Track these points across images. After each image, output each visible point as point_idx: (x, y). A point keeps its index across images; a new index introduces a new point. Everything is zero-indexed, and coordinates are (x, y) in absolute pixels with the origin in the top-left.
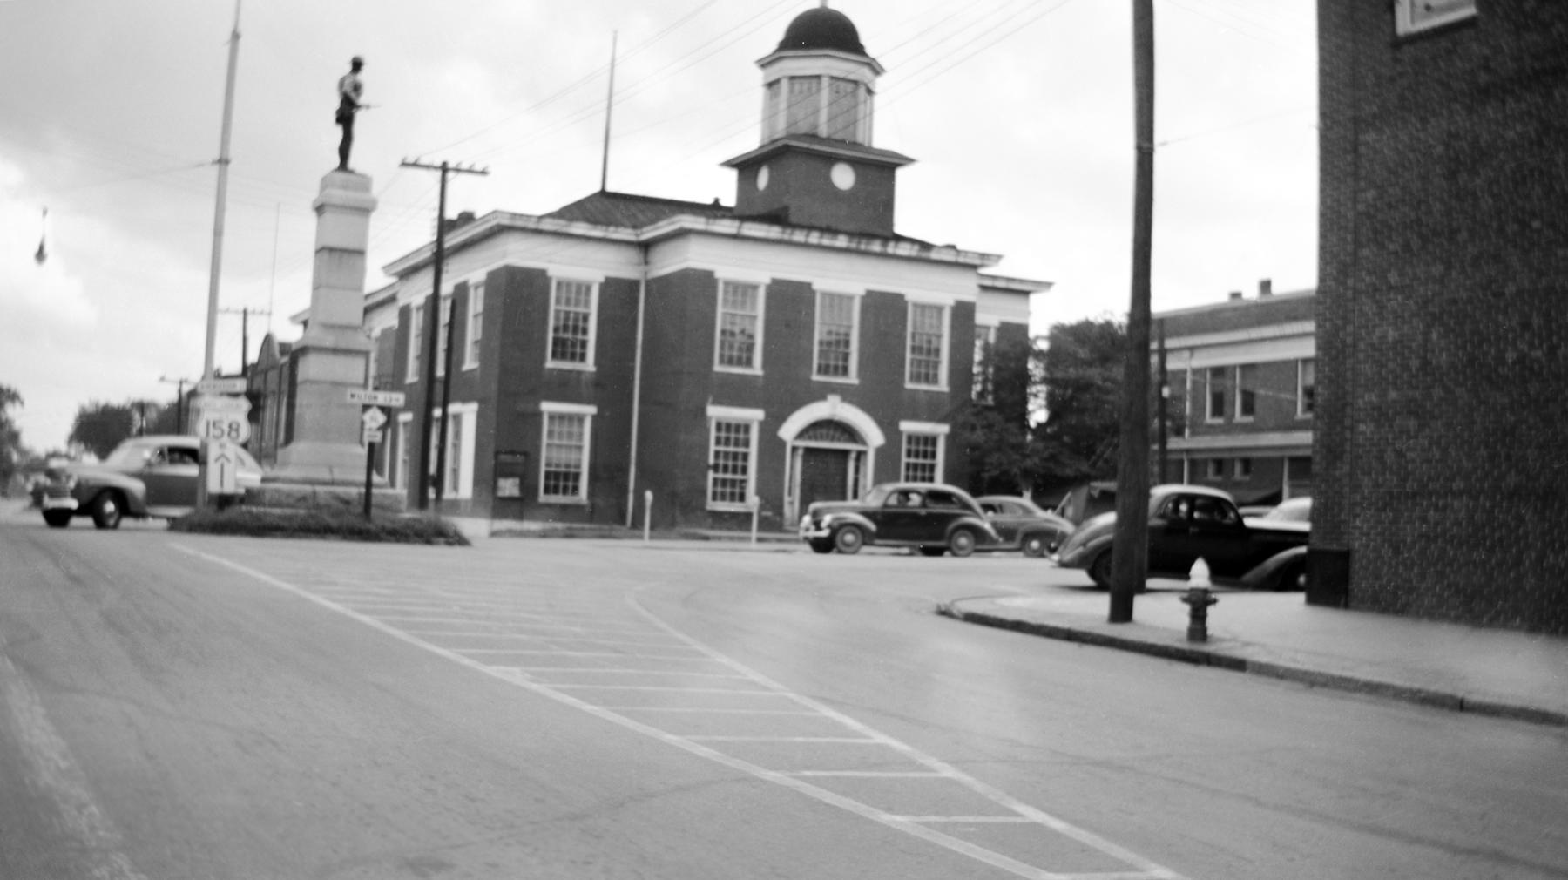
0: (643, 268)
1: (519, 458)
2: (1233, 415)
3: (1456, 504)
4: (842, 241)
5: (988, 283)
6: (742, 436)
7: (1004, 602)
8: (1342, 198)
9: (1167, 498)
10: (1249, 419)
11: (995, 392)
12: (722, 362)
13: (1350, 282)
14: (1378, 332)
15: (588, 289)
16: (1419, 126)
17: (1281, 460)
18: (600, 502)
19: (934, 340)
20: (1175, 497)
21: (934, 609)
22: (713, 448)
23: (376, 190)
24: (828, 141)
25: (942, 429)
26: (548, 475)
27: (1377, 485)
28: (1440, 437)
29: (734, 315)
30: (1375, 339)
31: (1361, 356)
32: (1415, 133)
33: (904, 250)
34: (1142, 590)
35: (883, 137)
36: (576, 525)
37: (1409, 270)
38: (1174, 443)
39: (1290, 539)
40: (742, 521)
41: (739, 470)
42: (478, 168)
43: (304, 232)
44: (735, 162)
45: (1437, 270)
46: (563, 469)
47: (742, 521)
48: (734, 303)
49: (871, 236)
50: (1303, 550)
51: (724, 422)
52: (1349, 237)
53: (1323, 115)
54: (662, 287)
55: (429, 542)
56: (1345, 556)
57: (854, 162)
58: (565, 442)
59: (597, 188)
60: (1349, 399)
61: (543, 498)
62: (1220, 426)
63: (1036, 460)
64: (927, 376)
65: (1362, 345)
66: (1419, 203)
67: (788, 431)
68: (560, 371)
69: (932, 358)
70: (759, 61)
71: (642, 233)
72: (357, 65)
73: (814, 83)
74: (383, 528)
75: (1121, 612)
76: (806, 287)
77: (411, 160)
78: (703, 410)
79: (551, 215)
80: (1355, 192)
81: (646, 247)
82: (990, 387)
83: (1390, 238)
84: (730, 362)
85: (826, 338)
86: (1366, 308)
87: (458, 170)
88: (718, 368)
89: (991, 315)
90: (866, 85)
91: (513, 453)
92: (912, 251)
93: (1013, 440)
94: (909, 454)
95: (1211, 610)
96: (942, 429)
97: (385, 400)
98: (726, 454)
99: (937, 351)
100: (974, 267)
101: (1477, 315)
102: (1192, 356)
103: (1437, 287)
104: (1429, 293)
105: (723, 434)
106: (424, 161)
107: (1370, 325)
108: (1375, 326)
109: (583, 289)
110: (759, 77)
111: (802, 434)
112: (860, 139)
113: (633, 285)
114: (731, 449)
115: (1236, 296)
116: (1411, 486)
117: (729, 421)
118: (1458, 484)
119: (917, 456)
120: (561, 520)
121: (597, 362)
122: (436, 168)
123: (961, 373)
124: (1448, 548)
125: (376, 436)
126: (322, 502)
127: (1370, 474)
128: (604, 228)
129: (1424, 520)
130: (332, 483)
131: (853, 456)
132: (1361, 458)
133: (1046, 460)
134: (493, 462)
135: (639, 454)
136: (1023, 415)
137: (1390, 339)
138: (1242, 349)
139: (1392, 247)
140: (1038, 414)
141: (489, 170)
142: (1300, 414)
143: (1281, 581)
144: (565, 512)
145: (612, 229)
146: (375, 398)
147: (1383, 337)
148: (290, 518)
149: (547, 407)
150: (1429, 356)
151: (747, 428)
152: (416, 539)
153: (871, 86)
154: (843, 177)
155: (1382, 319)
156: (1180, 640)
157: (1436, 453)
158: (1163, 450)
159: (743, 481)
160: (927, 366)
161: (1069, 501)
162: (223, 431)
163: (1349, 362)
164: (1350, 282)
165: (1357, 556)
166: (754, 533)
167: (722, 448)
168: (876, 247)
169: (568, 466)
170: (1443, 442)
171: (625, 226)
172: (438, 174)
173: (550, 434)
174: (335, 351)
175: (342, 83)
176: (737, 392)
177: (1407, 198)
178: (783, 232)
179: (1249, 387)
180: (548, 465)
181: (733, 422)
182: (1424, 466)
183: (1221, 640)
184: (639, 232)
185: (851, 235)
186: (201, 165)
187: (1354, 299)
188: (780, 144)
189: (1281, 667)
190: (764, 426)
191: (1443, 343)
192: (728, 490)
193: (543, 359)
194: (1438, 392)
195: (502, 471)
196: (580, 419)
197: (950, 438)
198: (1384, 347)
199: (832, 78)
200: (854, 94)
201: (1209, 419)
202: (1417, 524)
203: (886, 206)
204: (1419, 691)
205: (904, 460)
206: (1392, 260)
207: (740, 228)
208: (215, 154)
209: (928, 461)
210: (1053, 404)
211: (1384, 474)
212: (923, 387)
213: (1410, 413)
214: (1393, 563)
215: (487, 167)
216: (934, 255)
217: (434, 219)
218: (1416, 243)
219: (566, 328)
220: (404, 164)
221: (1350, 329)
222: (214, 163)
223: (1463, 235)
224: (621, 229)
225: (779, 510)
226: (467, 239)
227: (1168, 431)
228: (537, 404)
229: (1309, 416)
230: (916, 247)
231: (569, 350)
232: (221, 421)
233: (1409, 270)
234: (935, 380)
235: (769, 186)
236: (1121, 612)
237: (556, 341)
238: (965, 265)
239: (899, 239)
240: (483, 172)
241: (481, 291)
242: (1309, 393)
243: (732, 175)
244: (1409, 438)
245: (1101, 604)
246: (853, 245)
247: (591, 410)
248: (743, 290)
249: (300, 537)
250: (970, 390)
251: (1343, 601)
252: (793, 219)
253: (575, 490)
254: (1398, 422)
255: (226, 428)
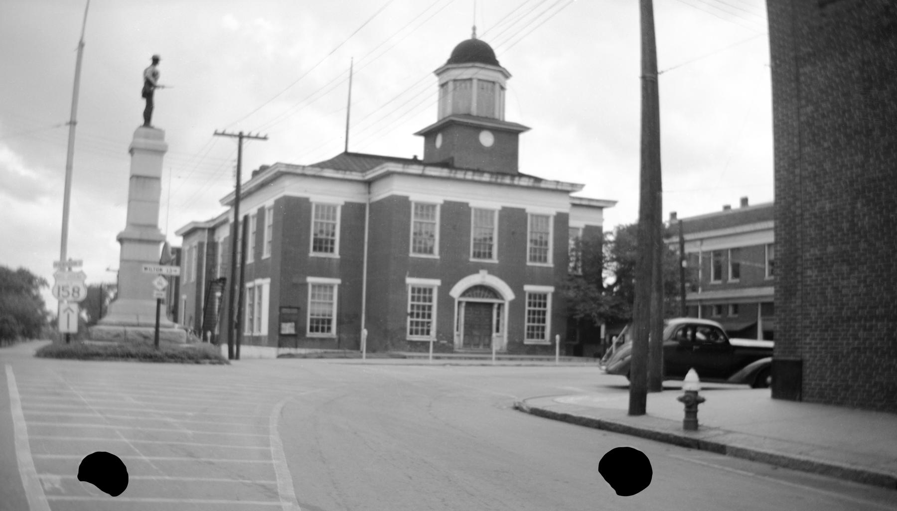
0: (367, 196)
1: (295, 311)
2: (727, 279)
3: (879, 324)
4: (486, 177)
5: (577, 202)
6: (427, 295)
7: (561, 400)
8: (789, 113)
9: (678, 327)
10: (737, 281)
11: (583, 266)
12: (414, 251)
13: (797, 171)
14: (818, 205)
15: (335, 211)
16: (841, 58)
17: (757, 304)
18: (344, 336)
19: (544, 236)
20: (684, 326)
21: (512, 405)
22: (410, 303)
23: (167, 139)
24: (477, 118)
25: (549, 290)
26: (312, 320)
27: (821, 313)
28: (866, 277)
29: (421, 223)
30: (816, 210)
31: (807, 222)
32: (838, 62)
33: (524, 182)
34: (658, 388)
35: (511, 115)
36: (329, 350)
37: (838, 160)
38: (690, 296)
39: (761, 353)
40: (424, 346)
41: (426, 316)
42: (262, 135)
43: (124, 167)
44: (423, 132)
45: (859, 158)
46: (321, 317)
47: (424, 346)
48: (422, 215)
49: (504, 174)
50: (768, 360)
51: (416, 287)
52: (796, 140)
53: (774, 57)
54: (378, 208)
55: (197, 363)
56: (799, 364)
57: (493, 130)
58: (322, 301)
59: (342, 150)
60: (799, 253)
61: (309, 334)
62: (719, 285)
63: (607, 308)
64: (540, 257)
65: (807, 215)
66: (844, 112)
67: (456, 291)
68: (318, 258)
69: (543, 247)
70: (435, 72)
71: (366, 175)
72: (156, 60)
73: (468, 84)
74: (166, 354)
75: (638, 407)
76: (465, 206)
77: (220, 131)
78: (403, 281)
79: (313, 166)
80: (798, 109)
81: (369, 183)
82: (580, 264)
83: (824, 139)
84: (420, 251)
85: (479, 237)
86: (809, 189)
87: (249, 137)
88: (412, 255)
89: (579, 221)
90: (500, 84)
91: (290, 307)
92: (530, 183)
93: (592, 295)
94: (530, 305)
95: (700, 407)
96: (549, 290)
97: (167, 271)
98: (418, 307)
99: (546, 243)
100: (568, 192)
101: (890, 188)
102: (702, 244)
103: (859, 171)
104: (854, 176)
105: (416, 295)
106: (228, 131)
107: (813, 200)
108: (816, 201)
109: (332, 208)
110: (435, 81)
111: (464, 294)
112: (497, 116)
113: (362, 207)
114: (421, 303)
115: (727, 208)
116: (845, 313)
117: (425, 287)
118: (880, 311)
119: (535, 306)
120: (320, 347)
121: (340, 254)
122: (235, 136)
123: (561, 256)
124: (874, 357)
125: (161, 295)
126: (130, 337)
127: (816, 305)
128: (343, 172)
129: (856, 338)
130: (138, 325)
131: (496, 306)
132: (809, 294)
133: (612, 307)
134: (278, 313)
135: (367, 307)
136: (600, 280)
137: (827, 209)
138: (732, 239)
139: (826, 145)
140: (609, 279)
141: (268, 136)
142: (767, 277)
143: (756, 381)
144: (323, 342)
145: (348, 173)
146: (161, 270)
147: (822, 209)
148: (106, 348)
149: (311, 280)
150: (856, 220)
151: (431, 291)
152: (189, 361)
153: (503, 85)
154: (487, 139)
155: (821, 195)
156: (678, 430)
157: (862, 289)
158: (684, 300)
159: (429, 323)
160: (540, 252)
161: (627, 331)
162: (69, 293)
163: (798, 228)
164: (797, 171)
165: (808, 364)
166: (431, 354)
167: (415, 303)
168: (507, 180)
169: (324, 315)
170: (868, 280)
171: (355, 170)
172: (237, 139)
173: (313, 296)
174: (141, 241)
175: (145, 72)
176: (423, 269)
177: (835, 109)
178: (451, 173)
179: (737, 261)
180: (312, 315)
181: (422, 287)
182: (855, 299)
183: (710, 429)
184: (364, 174)
185: (492, 173)
186: (58, 126)
187: (801, 183)
188: (447, 120)
189: (753, 452)
190: (440, 288)
191: (865, 209)
192: (420, 328)
193: (308, 251)
194: (863, 245)
195: (284, 319)
196: (331, 287)
197: (555, 295)
198: (823, 215)
199: (479, 80)
200: (493, 90)
201: (713, 281)
202: (851, 341)
203: (513, 156)
204: (862, 472)
205: (527, 308)
206: (827, 154)
207: (423, 170)
208: (68, 119)
209: (542, 309)
210: (621, 275)
211: (826, 305)
212: (538, 264)
213: (843, 261)
214: (835, 368)
215: (267, 135)
216: (543, 185)
217: (235, 167)
218: (843, 140)
219: (321, 232)
220: (216, 134)
221: (798, 203)
222: (67, 124)
223: (876, 133)
224: (354, 173)
225: (451, 340)
226: (263, 181)
227: (686, 289)
228: (305, 278)
229: (772, 278)
230: (532, 180)
231: (324, 246)
232: (68, 287)
233: (838, 160)
234: (545, 260)
235: (443, 146)
236: (638, 407)
237: (315, 241)
238: (561, 190)
239: (521, 175)
240: (265, 138)
241: (272, 212)
242: (772, 263)
243: (422, 140)
244: (843, 279)
245: (623, 400)
246: (493, 180)
247: (338, 281)
248: (426, 208)
249: (111, 360)
250: (567, 265)
251: (798, 397)
252: (457, 165)
253: (329, 329)
254: (835, 267)
255: (71, 291)
